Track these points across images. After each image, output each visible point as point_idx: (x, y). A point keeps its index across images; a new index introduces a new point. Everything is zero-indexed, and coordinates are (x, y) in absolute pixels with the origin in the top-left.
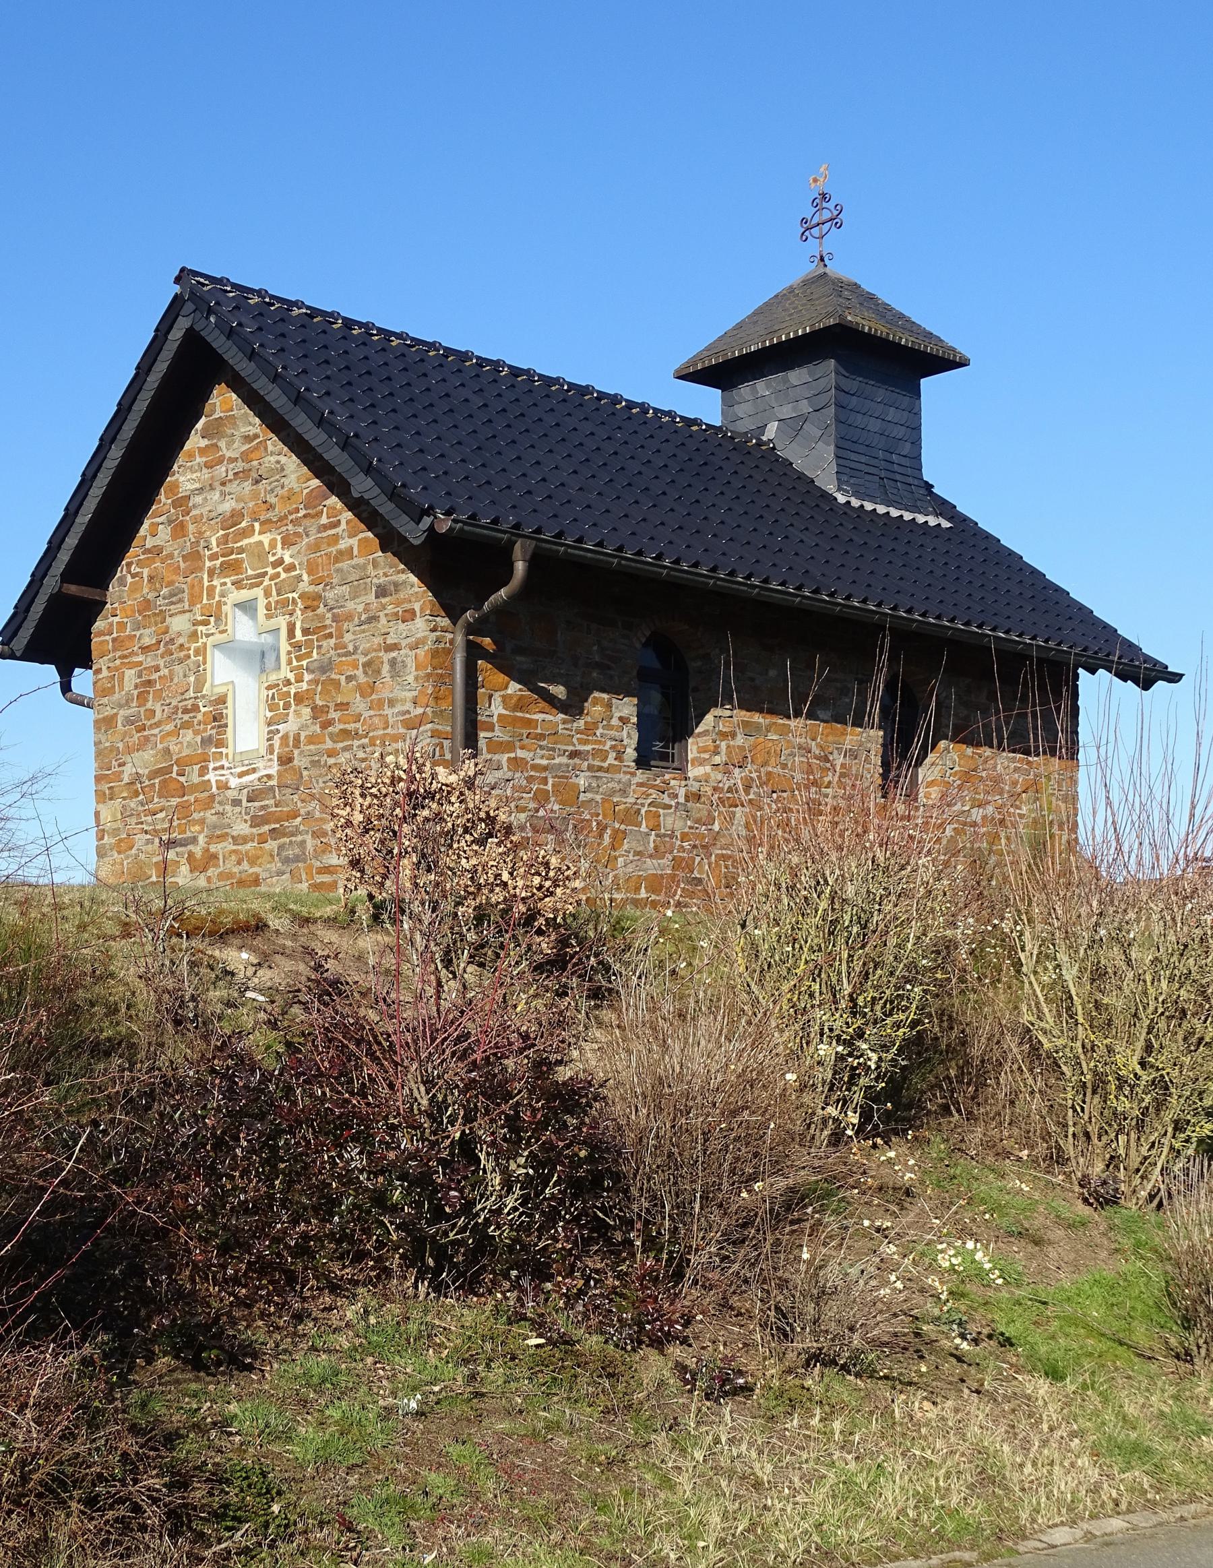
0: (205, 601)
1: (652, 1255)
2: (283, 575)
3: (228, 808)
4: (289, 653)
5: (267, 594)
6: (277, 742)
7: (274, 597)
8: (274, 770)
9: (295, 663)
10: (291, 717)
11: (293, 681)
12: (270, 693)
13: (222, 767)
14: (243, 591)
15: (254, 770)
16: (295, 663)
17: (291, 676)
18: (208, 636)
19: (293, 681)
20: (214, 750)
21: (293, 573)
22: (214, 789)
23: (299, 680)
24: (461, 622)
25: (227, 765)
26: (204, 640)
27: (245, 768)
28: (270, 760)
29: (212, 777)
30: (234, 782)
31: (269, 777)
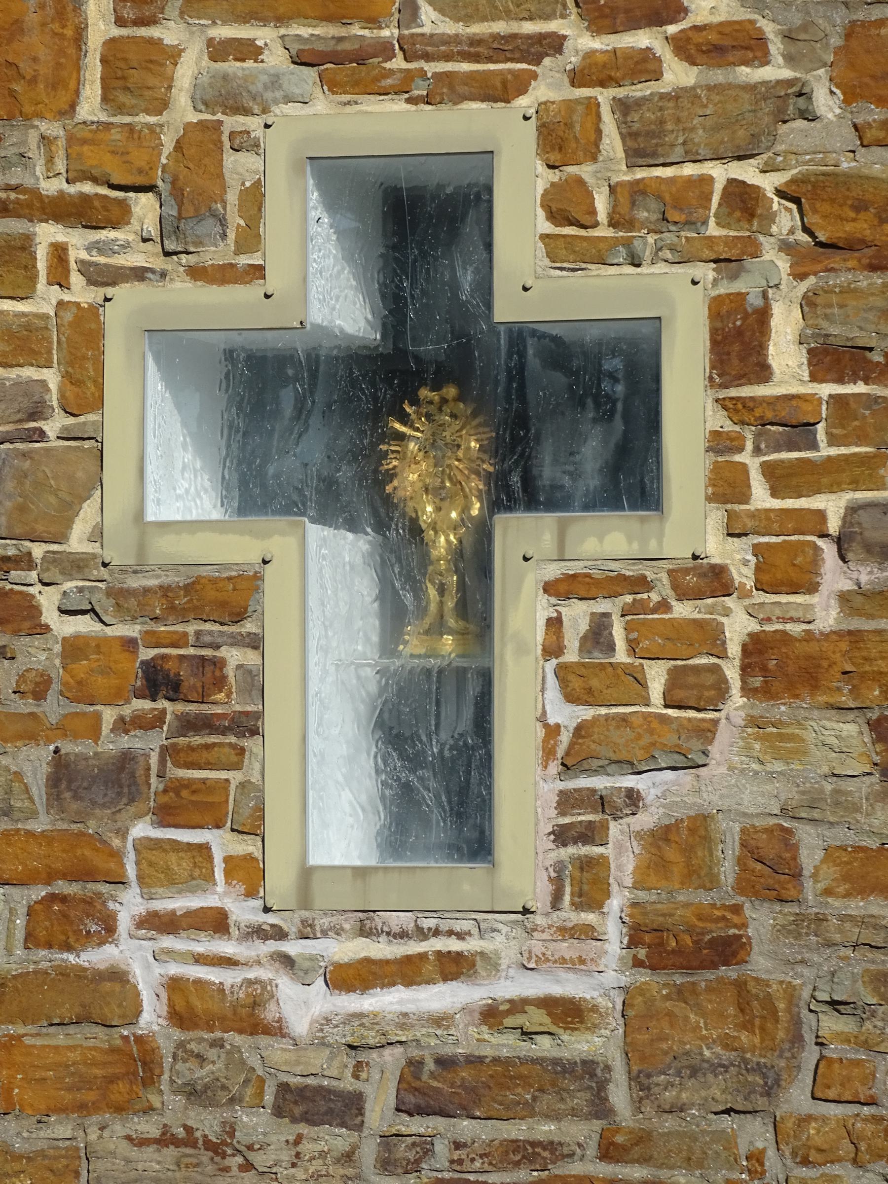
0: (90, 106)
1: (403, 780)
2: (678, 74)
3: (254, 1122)
4: (720, 444)
5: (561, 138)
6: (621, 851)
7: (609, 166)
8: (604, 976)
9: (761, 497)
10: (725, 748)
11: (743, 576)
12: (577, 615)
13: (217, 922)
14: (372, 105)
15: (454, 967)
16: (761, 497)
17: (738, 558)
18: (102, 277)
19: (743, 576)
20: (142, 829)
21: (747, 74)
22: (151, 1017)
23: (782, 573)
24: (634, 951)
25: (243, 912)
26: (80, 292)
27: (381, 949)
28: (588, 933)
29: (142, 963)
30: (304, 1006)
31: (569, 1013)
